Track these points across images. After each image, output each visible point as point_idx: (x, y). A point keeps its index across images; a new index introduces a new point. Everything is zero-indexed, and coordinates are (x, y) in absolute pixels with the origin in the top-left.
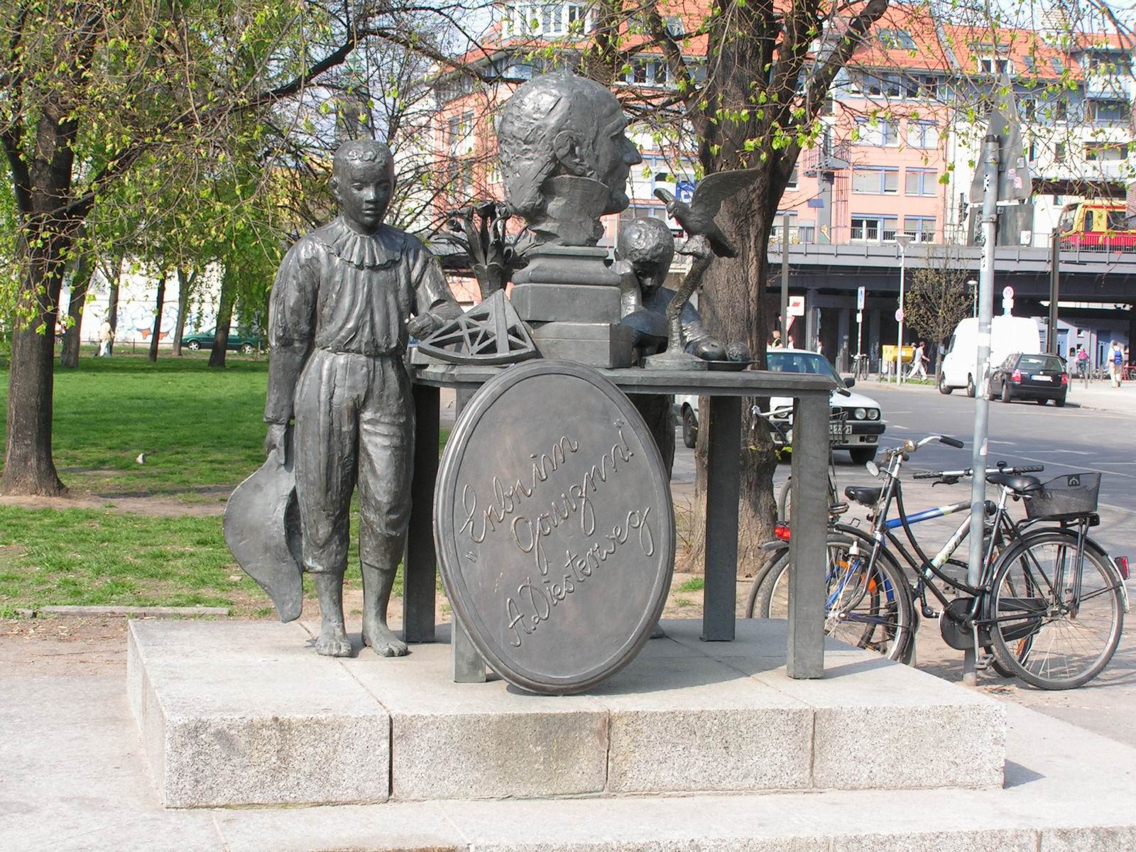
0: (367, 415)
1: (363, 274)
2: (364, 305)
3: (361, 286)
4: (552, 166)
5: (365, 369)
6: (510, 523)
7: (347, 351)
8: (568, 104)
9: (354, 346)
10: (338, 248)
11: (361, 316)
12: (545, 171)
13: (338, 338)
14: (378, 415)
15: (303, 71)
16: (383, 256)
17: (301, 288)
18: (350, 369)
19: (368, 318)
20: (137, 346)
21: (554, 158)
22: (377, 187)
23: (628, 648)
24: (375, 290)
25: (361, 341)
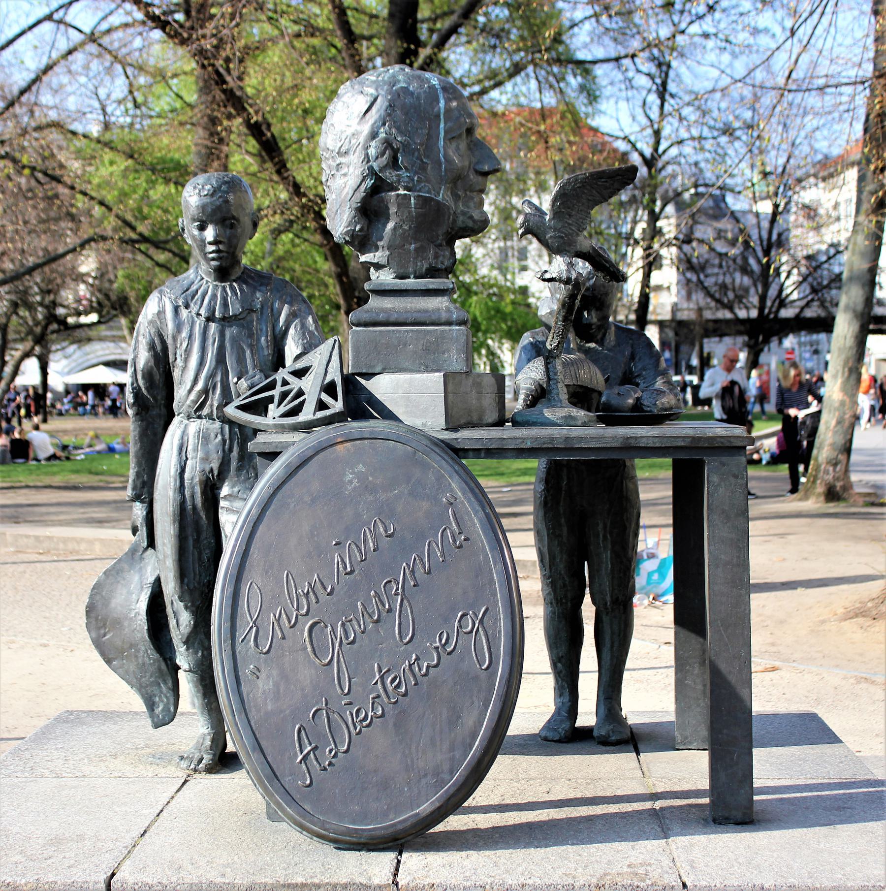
0: (225, 491)
1: (213, 326)
2: (214, 363)
3: (211, 340)
4: (370, 182)
5: (219, 437)
6: (303, 631)
7: (200, 417)
8: (387, 104)
9: (206, 411)
10: (186, 299)
11: (211, 376)
12: (363, 188)
13: (188, 402)
14: (236, 489)
15: (34, 88)
16: (238, 306)
17: (152, 347)
18: (204, 437)
19: (219, 378)
20: (717, 339)
21: (372, 172)
22: (216, 223)
23: (452, 791)
24: (228, 345)
25: (212, 406)
